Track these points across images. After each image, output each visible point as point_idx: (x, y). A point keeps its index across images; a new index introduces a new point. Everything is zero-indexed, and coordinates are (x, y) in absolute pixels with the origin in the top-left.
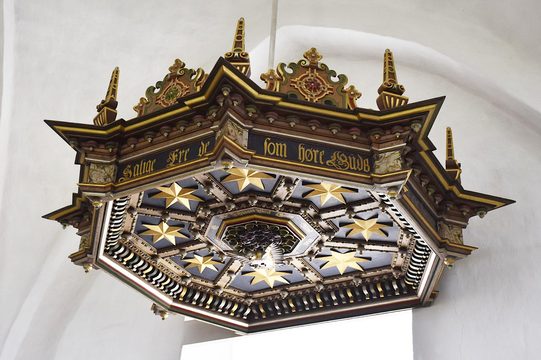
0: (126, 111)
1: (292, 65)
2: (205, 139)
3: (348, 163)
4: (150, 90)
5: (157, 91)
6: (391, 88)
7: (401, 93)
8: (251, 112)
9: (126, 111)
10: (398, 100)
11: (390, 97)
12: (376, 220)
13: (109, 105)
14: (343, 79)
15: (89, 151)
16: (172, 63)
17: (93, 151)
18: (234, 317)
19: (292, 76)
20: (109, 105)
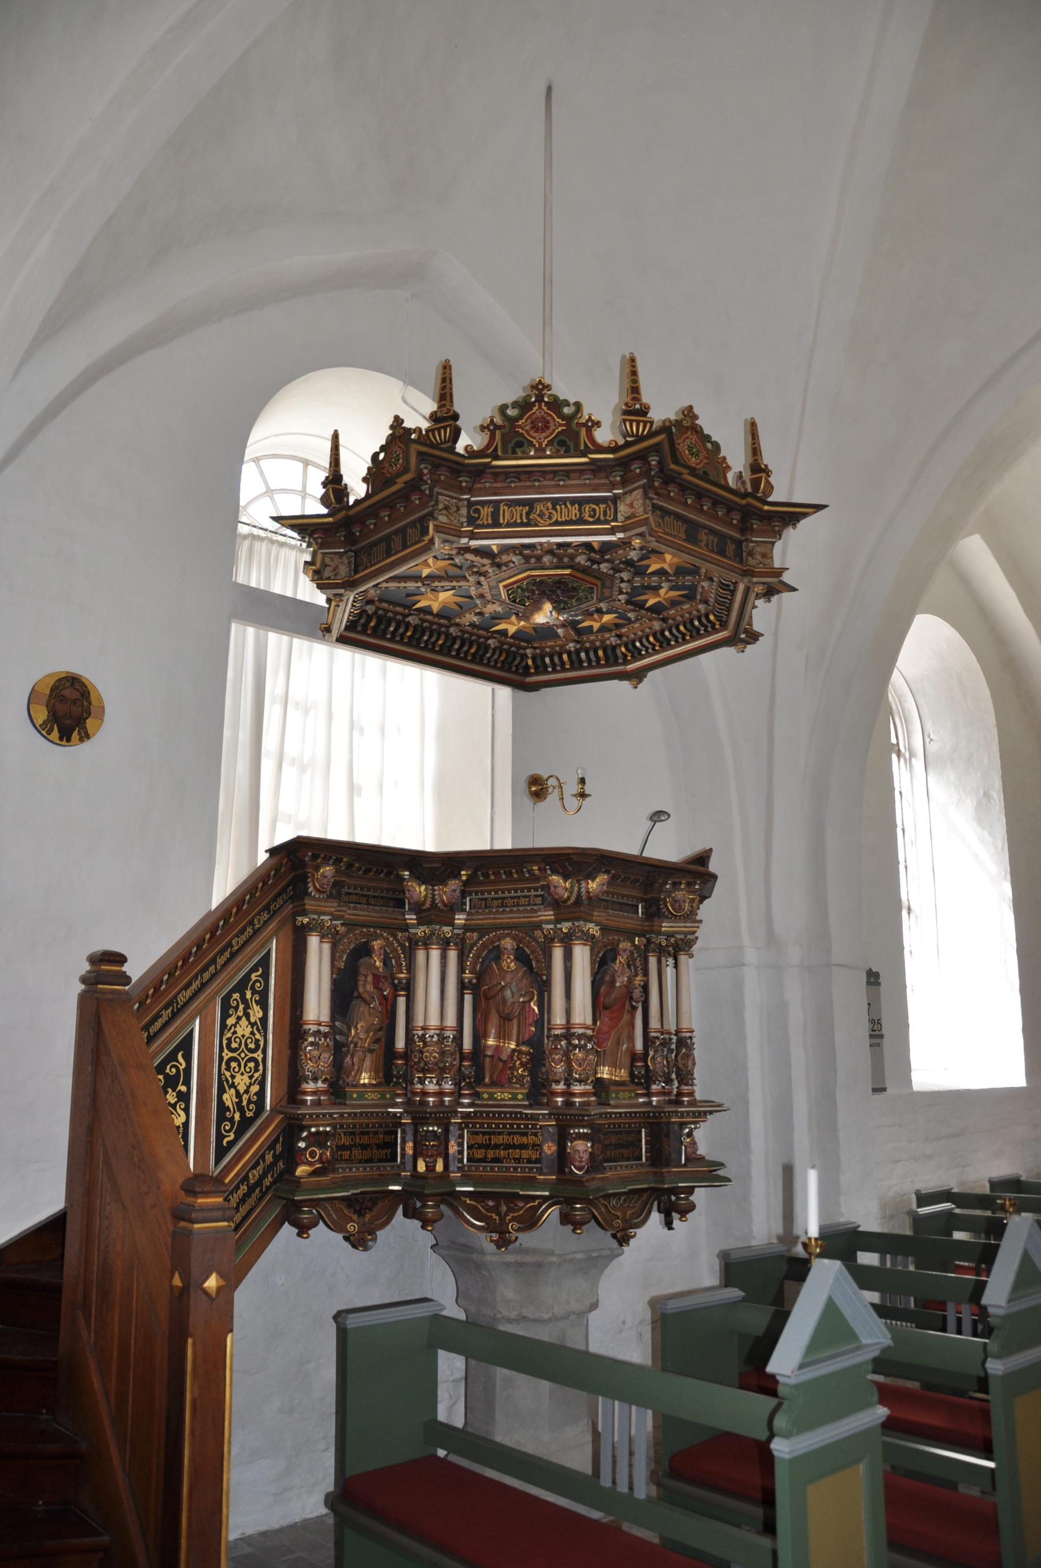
0: (357, 489)
1: (515, 404)
2: (396, 532)
3: (549, 522)
4: (375, 456)
5: (382, 456)
6: (634, 410)
7: (645, 414)
8: (464, 481)
9: (357, 489)
10: (641, 424)
11: (631, 422)
12: (451, 562)
13: (334, 482)
14: (578, 406)
15: (486, 1036)
16: (390, 421)
17: (246, 1178)
18: (472, 661)
19: (517, 419)
20: (334, 482)
